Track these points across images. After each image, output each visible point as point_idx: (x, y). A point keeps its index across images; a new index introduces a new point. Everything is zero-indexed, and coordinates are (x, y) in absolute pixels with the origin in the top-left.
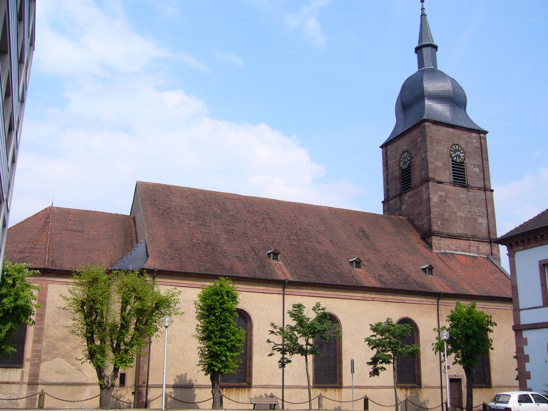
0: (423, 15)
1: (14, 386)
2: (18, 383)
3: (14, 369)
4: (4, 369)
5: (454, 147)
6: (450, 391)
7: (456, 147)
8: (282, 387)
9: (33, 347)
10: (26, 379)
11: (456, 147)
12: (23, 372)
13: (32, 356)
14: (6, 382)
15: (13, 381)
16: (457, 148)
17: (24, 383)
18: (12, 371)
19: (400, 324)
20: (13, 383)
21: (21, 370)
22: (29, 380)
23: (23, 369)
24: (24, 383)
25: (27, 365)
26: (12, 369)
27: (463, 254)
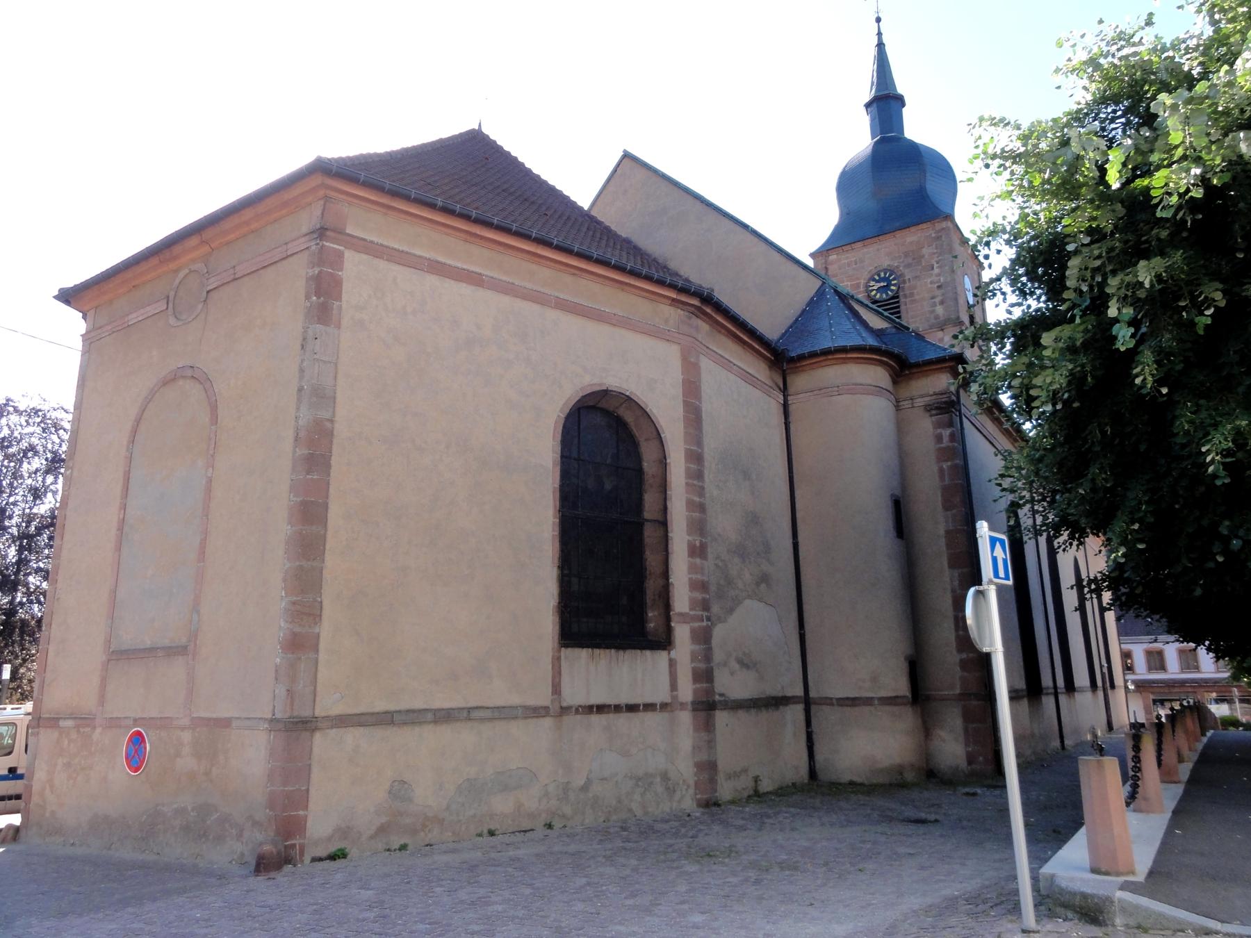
0: (881, 46)
1: (650, 718)
2: (664, 706)
3: (644, 651)
4: (613, 651)
5: (895, 282)
6: (562, 551)
7: (894, 285)
8: (1053, 691)
9: (693, 569)
10: (687, 691)
11: (894, 285)
12: (672, 663)
13: (694, 604)
14: (812, 732)
15: (649, 700)
16: (893, 288)
17: (683, 706)
18: (639, 661)
19: (1208, 665)
20: (649, 707)
21: (664, 654)
22: (695, 692)
23: (673, 653)
24: (683, 706)
25: (682, 633)
26: (639, 651)
27: (443, 221)
